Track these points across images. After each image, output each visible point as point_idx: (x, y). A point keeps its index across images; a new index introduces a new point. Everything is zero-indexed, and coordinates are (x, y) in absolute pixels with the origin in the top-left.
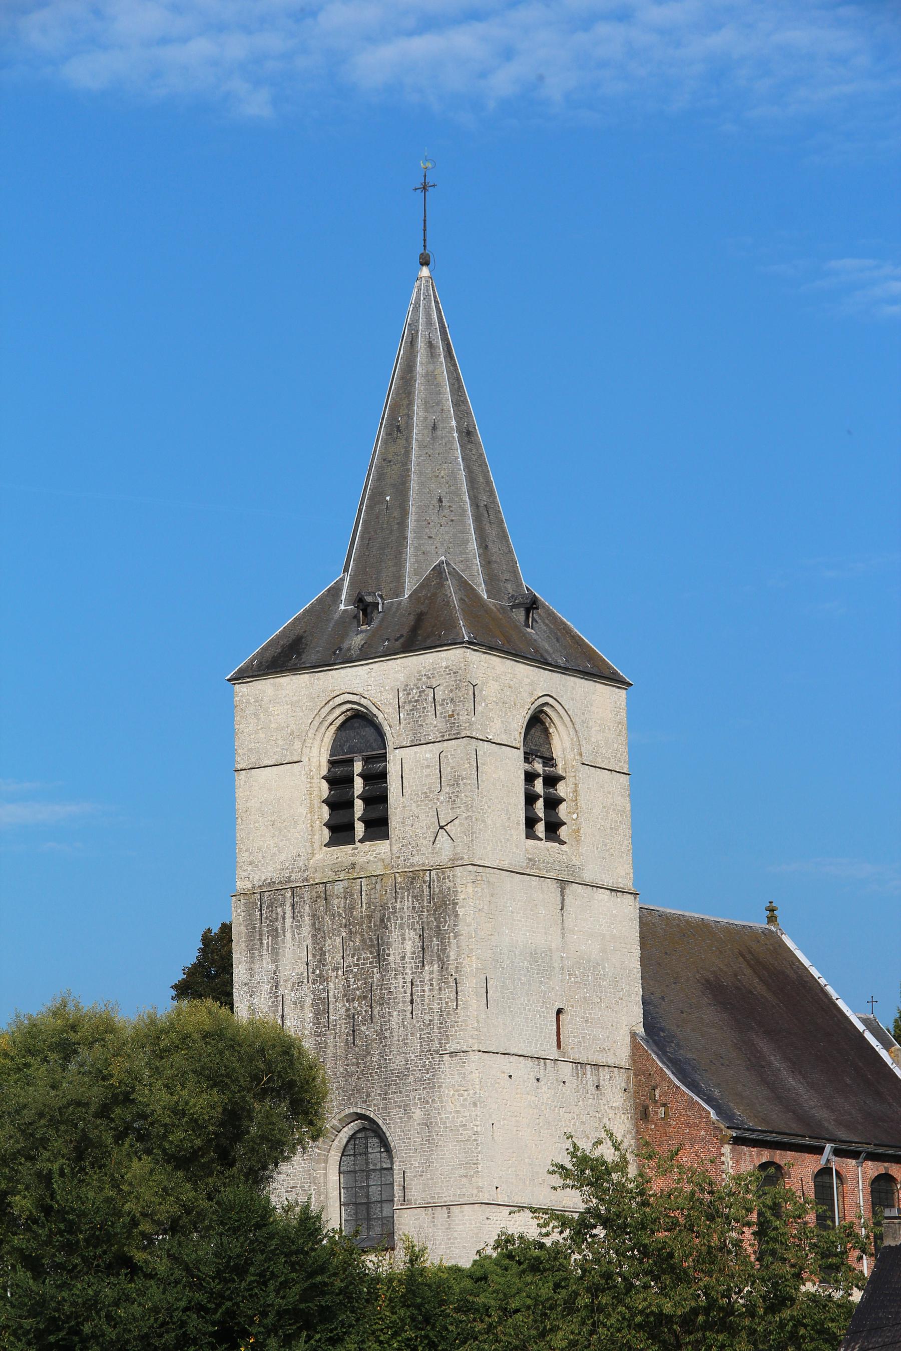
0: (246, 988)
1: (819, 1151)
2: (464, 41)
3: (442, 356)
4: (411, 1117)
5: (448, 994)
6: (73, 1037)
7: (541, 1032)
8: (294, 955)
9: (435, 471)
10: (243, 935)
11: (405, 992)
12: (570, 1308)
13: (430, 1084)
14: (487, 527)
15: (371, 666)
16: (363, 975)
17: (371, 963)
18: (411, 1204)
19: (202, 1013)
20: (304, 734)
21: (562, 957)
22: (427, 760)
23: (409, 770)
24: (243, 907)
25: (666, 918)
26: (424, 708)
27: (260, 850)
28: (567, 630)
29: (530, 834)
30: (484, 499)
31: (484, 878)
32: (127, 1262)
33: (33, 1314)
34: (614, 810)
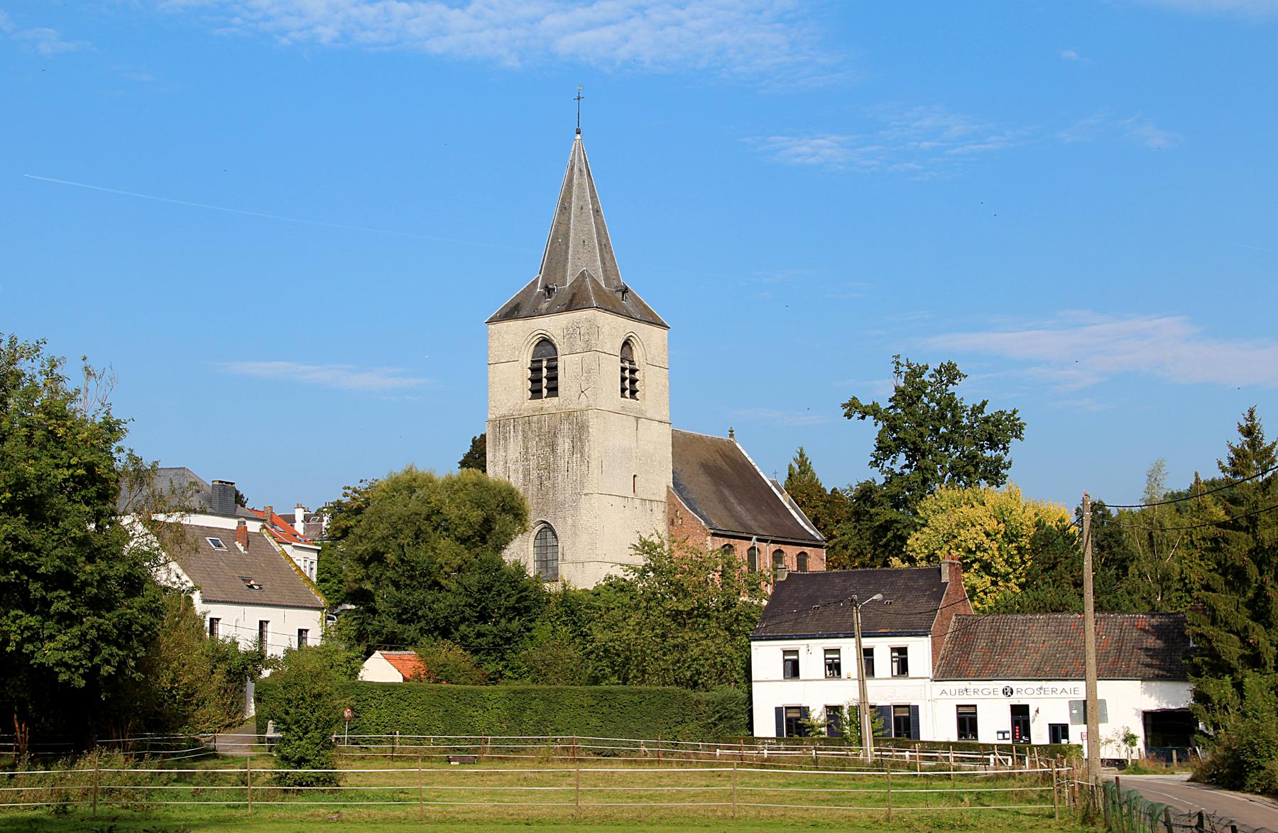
1: (750, 539)
2: (607, 34)
5: (584, 468)
6: (414, 484)
8: (514, 448)
9: (582, 228)
12: (637, 608)
13: (576, 508)
16: (546, 459)
19: (473, 474)
25: (684, 435)
28: (642, 303)
29: (623, 396)
30: (604, 241)
32: (437, 583)
33: (396, 606)
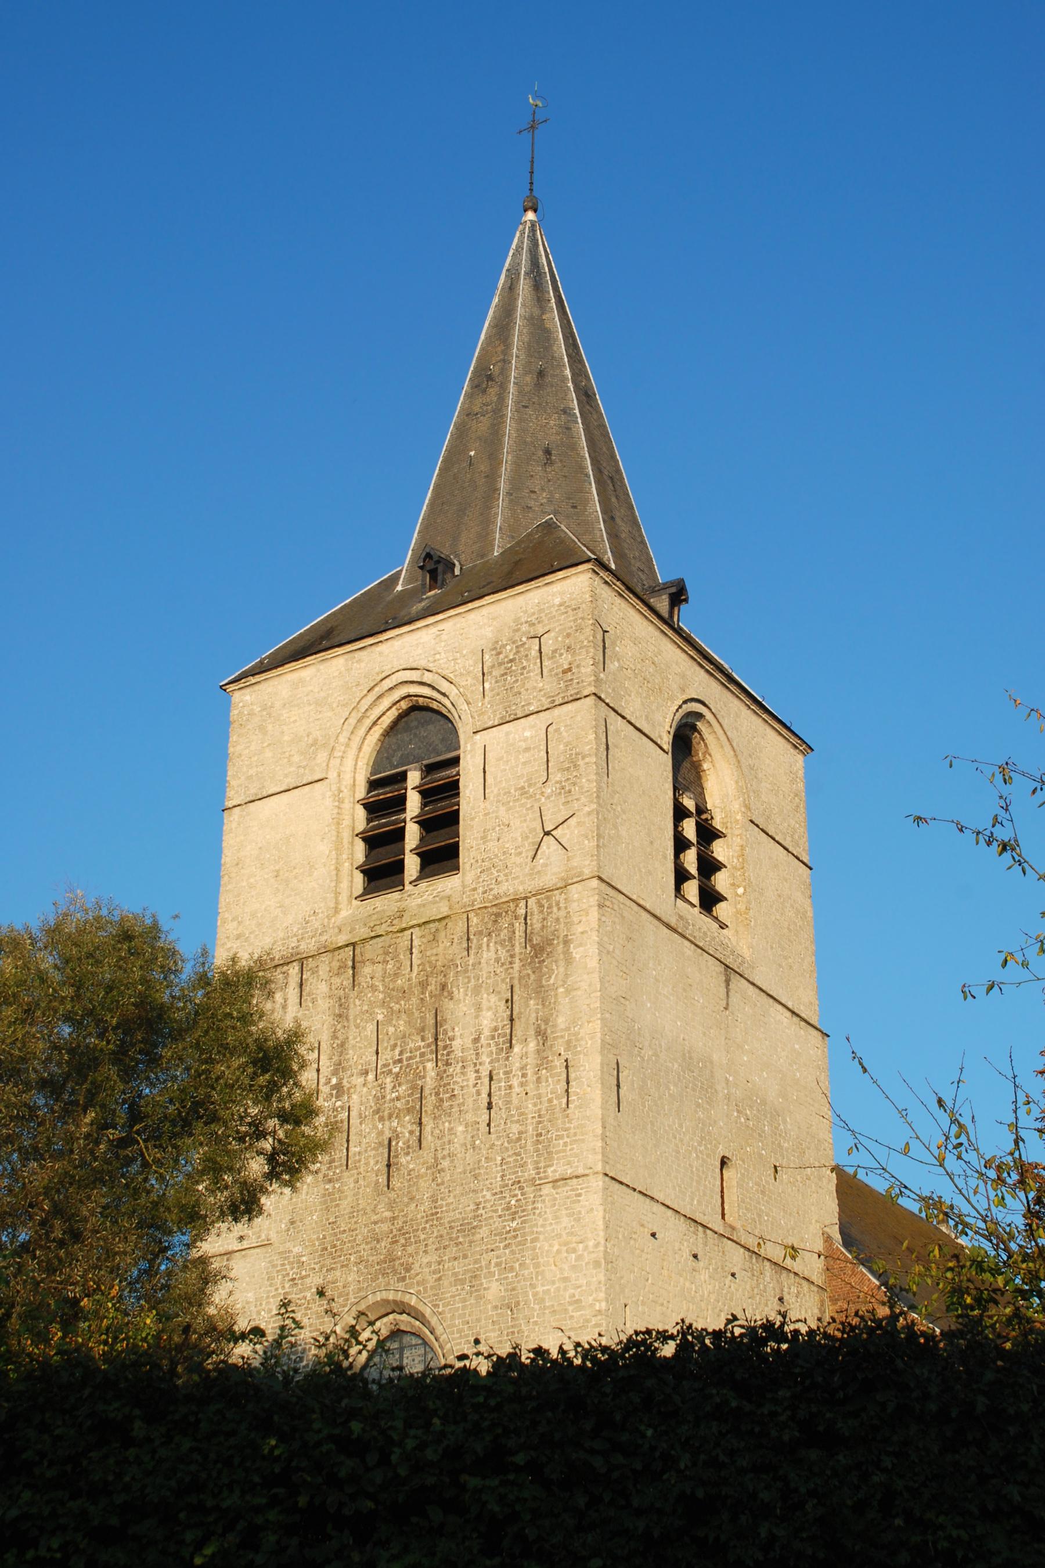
4: (480, 1298)
5: (553, 1085)
11: (478, 1093)
15: (440, 626)
17: (422, 1055)
21: (727, 1080)
22: (525, 740)
23: (494, 769)
26: (524, 668)
27: (253, 915)
31: (616, 907)
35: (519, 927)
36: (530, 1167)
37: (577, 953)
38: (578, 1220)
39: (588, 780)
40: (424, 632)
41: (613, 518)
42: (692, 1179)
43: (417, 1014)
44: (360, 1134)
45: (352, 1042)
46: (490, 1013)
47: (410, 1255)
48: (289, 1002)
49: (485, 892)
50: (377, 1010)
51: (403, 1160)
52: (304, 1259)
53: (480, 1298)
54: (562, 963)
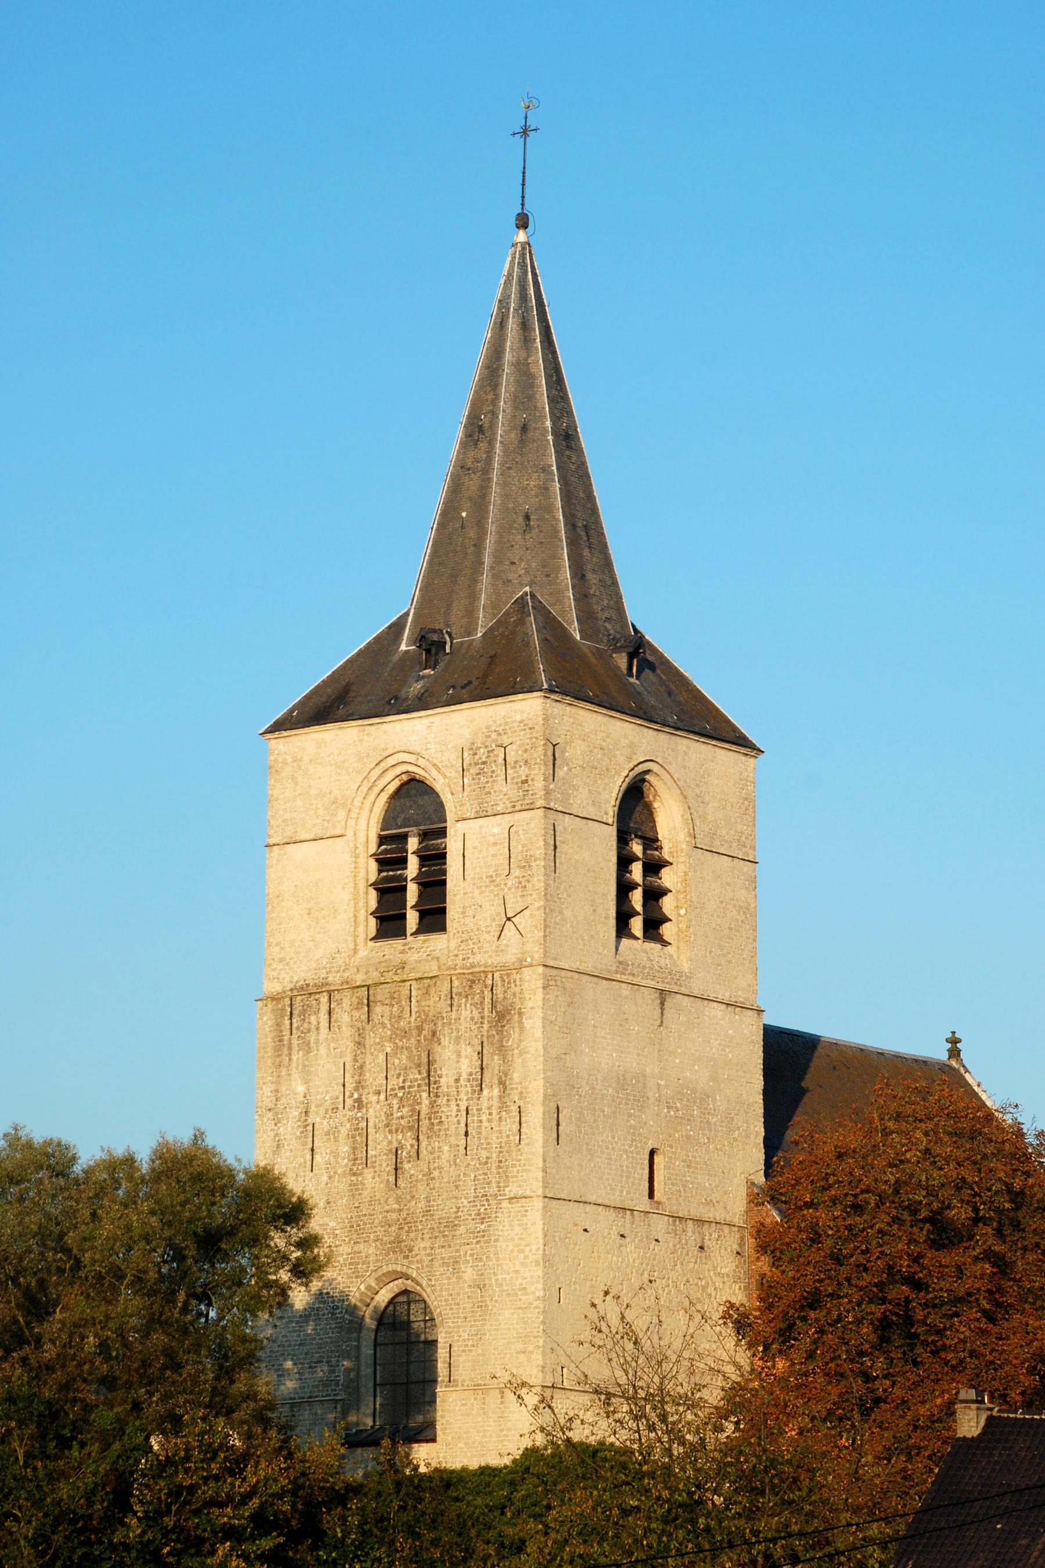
0: (270, 1115)
3: (538, 340)
5: (510, 1126)
7: (628, 1177)
10: (269, 1049)
11: (459, 1123)
13: (482, 1237)
14: (586, 552)
15: (431, 719)
17: (419, 1086)
18: (456, 1386)
20: (349, 802)
21: (659, 1085)
22: (494, 835)
23: (474, 848)
24: (270, 1015)
26: (493, 772)
31: (559, 983)
34: (735, 906)
35: (487, 993)
36: (494, 1185)
37: (527, 1024)
38: (526, 1229)
39: (538, 881)
40: (418, 721)
41: (583, 576)
42: (622, 1176)
43: (415, 1052)
44: (375, 1140)
45: (368, 1066)
46: (466, 1061)
47: (412, 1240)
48: (321, 1024)
49: (464, 959)
50: (386, 1044)
51: (406, 1166)
52: (337, 1232)
53: (459, 1278)
54: (517, 1030)
